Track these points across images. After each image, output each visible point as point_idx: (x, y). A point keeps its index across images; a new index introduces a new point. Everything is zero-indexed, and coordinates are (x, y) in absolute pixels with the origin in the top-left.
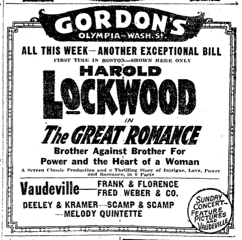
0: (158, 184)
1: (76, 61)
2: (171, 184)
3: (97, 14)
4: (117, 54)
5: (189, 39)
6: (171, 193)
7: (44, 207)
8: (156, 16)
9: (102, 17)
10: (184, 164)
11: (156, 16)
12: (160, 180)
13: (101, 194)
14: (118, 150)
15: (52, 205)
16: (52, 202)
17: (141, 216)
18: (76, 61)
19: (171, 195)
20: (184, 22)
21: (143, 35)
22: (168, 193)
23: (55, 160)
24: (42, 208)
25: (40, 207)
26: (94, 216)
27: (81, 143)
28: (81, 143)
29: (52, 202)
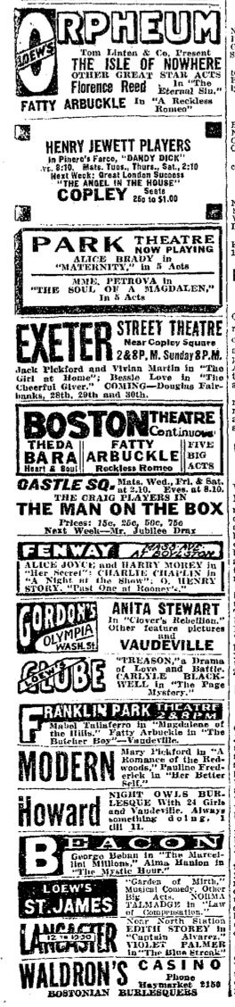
0: (79, 104)
1: (22, 513)
6: (69, 195)
7: (121, 107)
10: (45, 109)
12: (145, 408)
13: (26, 109)
14: (87, 108)
15: (55, 106)
17: (124, 107)
18: (22, 513)
19: (69, 199)
22: (64, 195)
24: (117, 107)
25: (114, 107)
26: (53, 109)
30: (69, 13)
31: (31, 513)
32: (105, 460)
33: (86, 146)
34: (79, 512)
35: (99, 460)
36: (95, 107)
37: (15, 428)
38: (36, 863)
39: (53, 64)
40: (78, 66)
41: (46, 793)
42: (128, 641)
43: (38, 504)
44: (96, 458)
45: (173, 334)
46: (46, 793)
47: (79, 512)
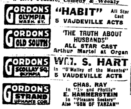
16: (106, 83)
29: (106, 83)
30: (116, 57)
31: (80, 83)
32: (119, 65)
33: (36, 102)
34: (107, 64)
35: (115, 65)
36: (111, 36)
37: (3, 65)
38: (114, 106)
39: (51, 19)
40: (82, 34)
41: (113, 95)
42: (67, 19)
43: (80, 83)
44: (113, 63)
45: (81, 35)
46: (113, 95)
47: (107, 64)
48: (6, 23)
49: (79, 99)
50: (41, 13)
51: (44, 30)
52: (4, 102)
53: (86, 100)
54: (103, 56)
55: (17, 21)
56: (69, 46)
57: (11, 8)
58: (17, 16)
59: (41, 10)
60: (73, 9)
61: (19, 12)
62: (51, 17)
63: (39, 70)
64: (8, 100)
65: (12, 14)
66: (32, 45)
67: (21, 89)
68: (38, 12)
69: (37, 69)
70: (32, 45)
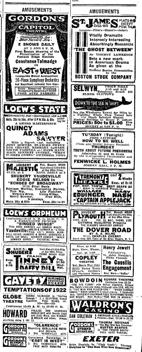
2: (84, 123)
3: (104, 303)
4: (92, 90)
5: (126, 100)
6: (79, 258)
8: (119, 303)
9: (106, 304)
11: (119, 303)
15: (97, 258)
20: (34, 107)
21: (25, 214)
23: (86, 160)
27: (72, 25)
28: (72, 25)
48: (4, 333)
49: (86, 258)
50: (21, 341)
51: (23, 337)
52: (4, 346)
53: (47, 44)
54: (134, 194)
55: (9, 332)
56: (28, 134)
57: (6, 338)
58: (9, 342)
59: (21, 339)
60: (30, 170)
61: (10, 340)
62: (10, 65)
63: (21, 331)
64: (6, 344)
65: (7, 341)
66: (10, 165)
67: (12, 339)
68: (20, 340)
69: (20, 330)
70: (10, 165)
